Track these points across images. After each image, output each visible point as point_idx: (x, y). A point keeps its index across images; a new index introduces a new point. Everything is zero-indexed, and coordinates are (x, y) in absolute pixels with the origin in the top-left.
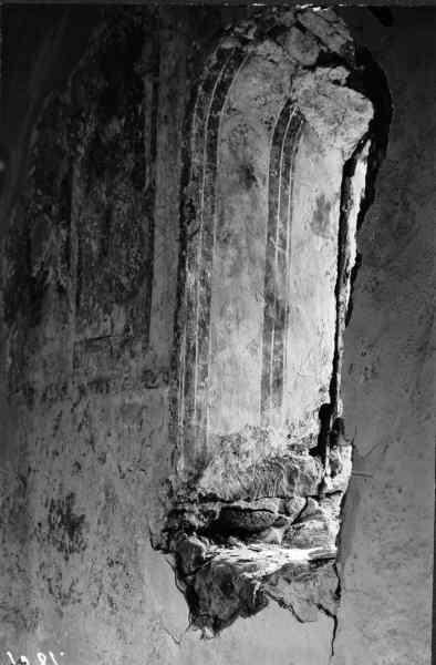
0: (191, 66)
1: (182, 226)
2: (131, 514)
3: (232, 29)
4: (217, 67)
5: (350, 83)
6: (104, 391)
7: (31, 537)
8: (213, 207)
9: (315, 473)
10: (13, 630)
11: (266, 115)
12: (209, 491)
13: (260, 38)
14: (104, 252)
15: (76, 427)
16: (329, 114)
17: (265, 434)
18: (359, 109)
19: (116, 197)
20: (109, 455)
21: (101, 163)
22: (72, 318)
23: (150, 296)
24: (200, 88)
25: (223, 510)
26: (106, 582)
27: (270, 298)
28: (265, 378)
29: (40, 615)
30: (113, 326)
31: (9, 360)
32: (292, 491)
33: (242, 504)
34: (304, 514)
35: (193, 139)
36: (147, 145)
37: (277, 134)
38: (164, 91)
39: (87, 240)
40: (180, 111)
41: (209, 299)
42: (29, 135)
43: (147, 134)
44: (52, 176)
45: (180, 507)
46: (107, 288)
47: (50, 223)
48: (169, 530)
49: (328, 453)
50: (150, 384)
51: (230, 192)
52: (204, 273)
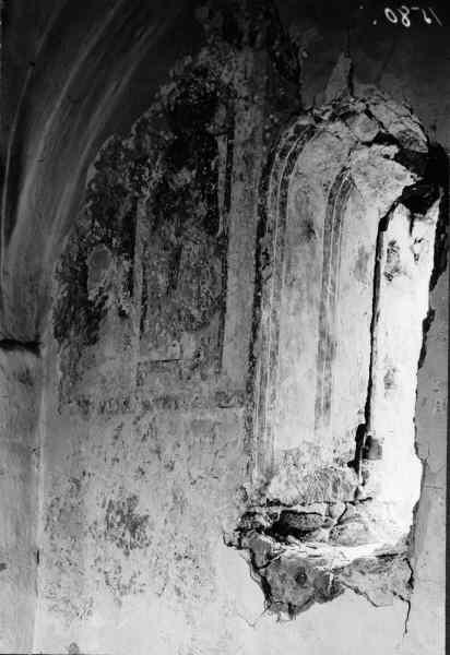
0: (268, 135)
1: (257, 271)
2: (202, 515)
3: (311, 109)
4: (293, 139)
5: (396, 158)
6: (173, 406)
7: (85, 534)
8: (282, 255)
9: (353, 483)
10: (63, 619)
11: (324, 179)
12: (275, 497)
13: (332, 119)
14: (173, 285)
15: (141, 438)
16: (373, 181)
17: (317, 448)
18: (399, 178)
19: (187, 239)
20: (177, 464)
21: (168, 204)
22: (135, 341)
23: (223, 328)
24: (277, 155)
25: (283, 512)
26: (173, 573)
27: (323, 334)
28: (318, 400)
29: (94, 605)
30: (182, 352)
31: (60, 374)
32: (336, 497)
33: (299, 508)
34: (344, 517)
35: (269, 198)
36: (221, 197)
37: (331, 196)
38: (239, 152)
39: (153, 273)
40: (257, 172)
41: (278, 333)
42: (84, 171)
43: (220, 188)
44: (112, 212)
45: (252, 510)
46: (175, 316)
47: (110, 254)
48: (242, 530)
49: (361, 465)
50: (223, 404)
51: (296, 244)
52: (275, 312)
